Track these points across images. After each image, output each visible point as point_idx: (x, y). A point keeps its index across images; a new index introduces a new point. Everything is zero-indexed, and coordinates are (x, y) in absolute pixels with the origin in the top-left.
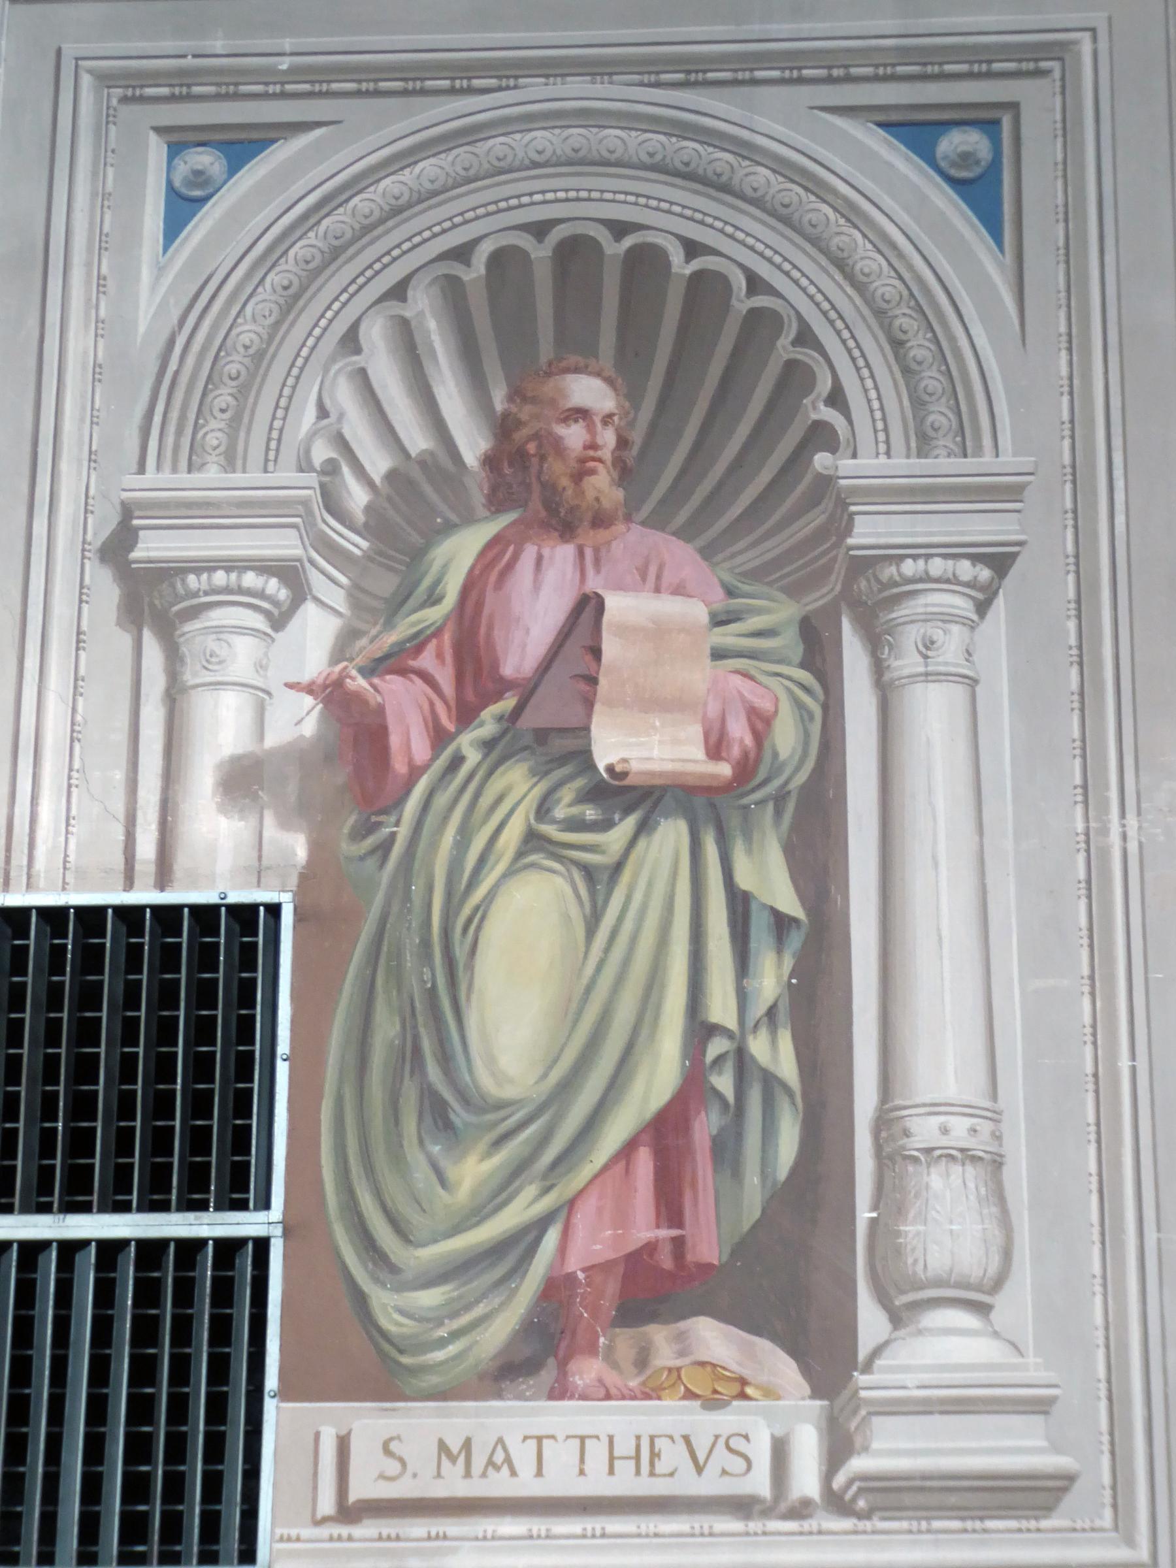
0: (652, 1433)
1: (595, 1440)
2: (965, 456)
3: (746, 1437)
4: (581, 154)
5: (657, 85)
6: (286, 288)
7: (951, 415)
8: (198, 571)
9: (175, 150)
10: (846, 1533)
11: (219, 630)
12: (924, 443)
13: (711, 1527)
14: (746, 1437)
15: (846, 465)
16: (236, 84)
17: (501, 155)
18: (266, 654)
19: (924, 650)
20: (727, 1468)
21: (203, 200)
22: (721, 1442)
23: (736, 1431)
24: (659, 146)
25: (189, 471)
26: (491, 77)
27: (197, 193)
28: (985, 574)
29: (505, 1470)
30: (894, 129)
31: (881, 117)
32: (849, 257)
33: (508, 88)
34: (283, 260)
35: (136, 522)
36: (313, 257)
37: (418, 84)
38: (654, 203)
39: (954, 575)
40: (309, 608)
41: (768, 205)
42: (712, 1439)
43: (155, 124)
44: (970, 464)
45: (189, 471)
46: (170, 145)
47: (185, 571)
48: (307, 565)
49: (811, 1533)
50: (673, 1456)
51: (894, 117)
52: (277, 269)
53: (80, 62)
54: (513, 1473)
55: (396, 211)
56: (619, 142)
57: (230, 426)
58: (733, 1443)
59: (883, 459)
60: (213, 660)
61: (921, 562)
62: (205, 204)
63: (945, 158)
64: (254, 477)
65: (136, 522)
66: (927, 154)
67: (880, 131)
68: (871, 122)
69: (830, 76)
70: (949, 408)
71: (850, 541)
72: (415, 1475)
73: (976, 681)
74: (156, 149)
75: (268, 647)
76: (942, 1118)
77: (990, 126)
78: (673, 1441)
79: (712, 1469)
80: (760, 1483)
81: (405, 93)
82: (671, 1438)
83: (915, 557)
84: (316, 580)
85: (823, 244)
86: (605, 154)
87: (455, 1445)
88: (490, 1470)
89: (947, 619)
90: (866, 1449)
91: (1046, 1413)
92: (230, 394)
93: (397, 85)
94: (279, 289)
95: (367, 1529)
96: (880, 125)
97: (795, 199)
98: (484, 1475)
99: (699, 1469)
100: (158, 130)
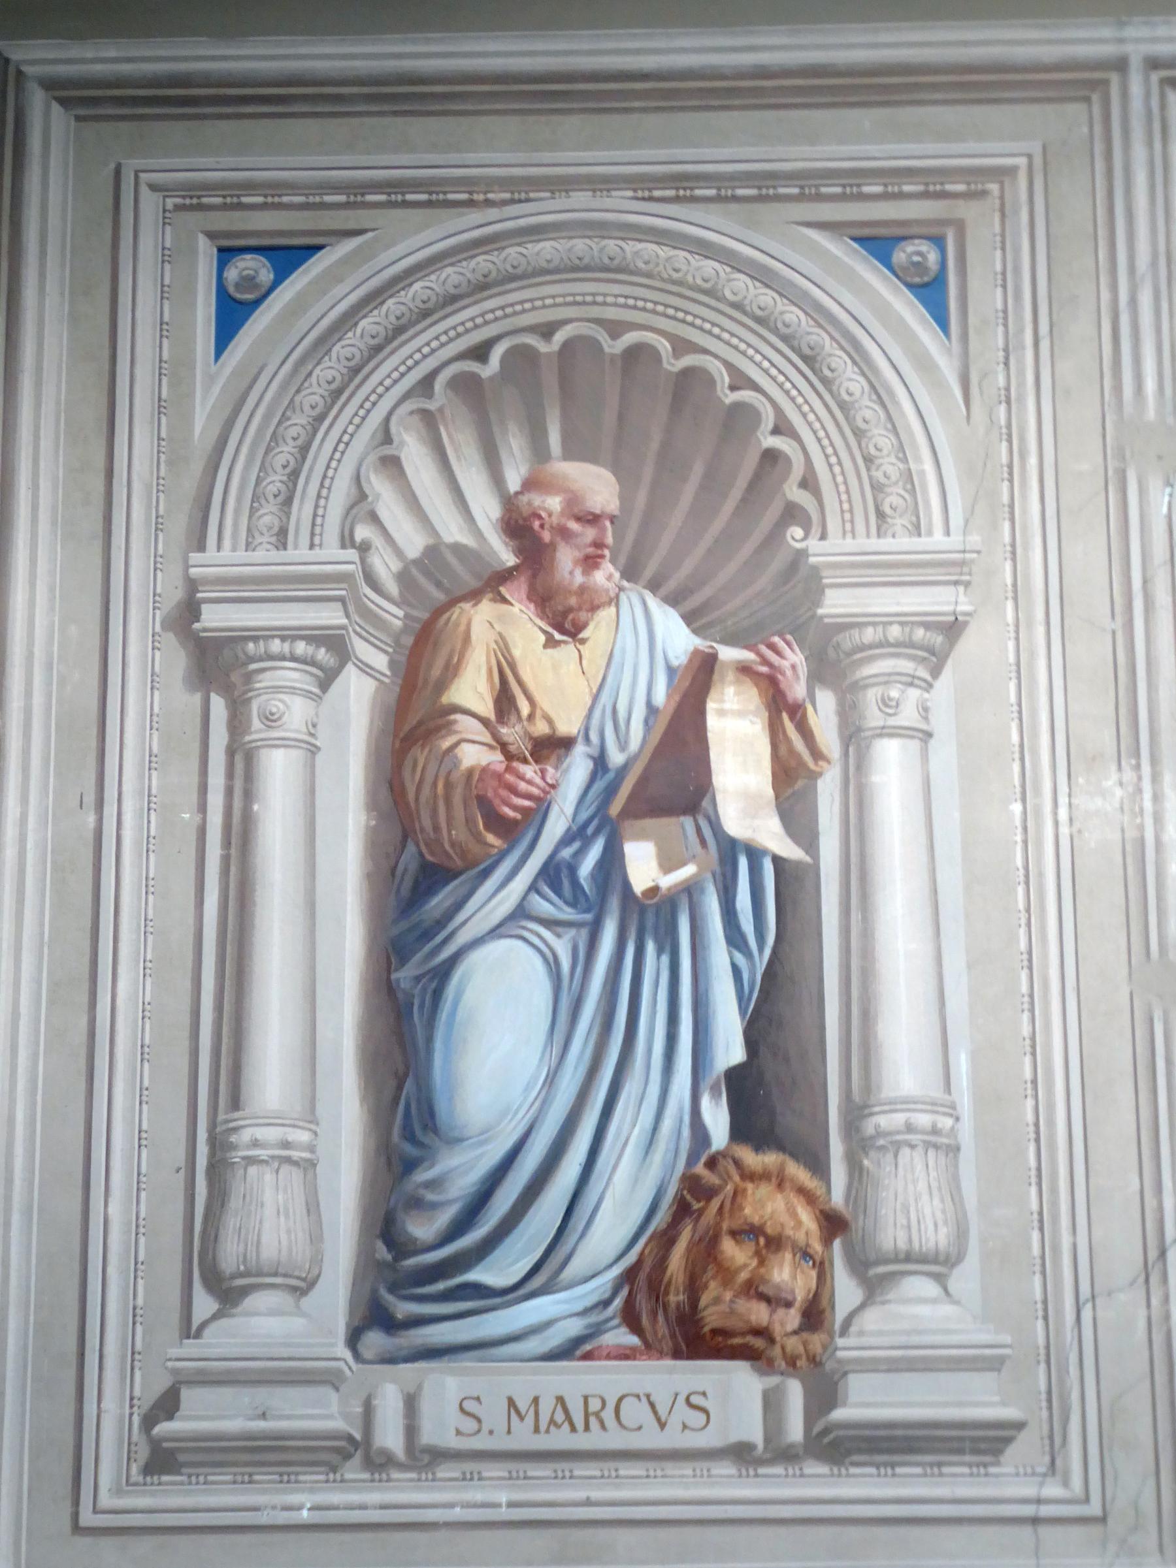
0: (585, 1392)
2: (919, 535)
4: (586, 261)
5: (651, 199)
6: (329, 383)
8: (255, 639)
9: (226, 254)
11: (278, 689)
13: (525, 1472)
15: (813, 544)
18: (317, 715)
21: (258, 302)
22: (681, 1400)
25: (246, 551)
26: (464, 192)
28: (938, 640)
29: (566, 1426)
30: (270, 253)
32: (818, 354)
33: (520, 201)
34: (327, 358)
35: (199, 595)
36: (354, 356)
37: (688, 193)
40: (350, 671)
41: (748, 308)
43: (210, 228)
44: (887, 543)
45: (246, 551)
46: (221, 250)
47: (861, 626)
48: (352, 634)
50: (635, 1412)
51: (866, 232)
53: (142, 175)
54: (573, 1429)
55: (425, 314)
57: (281, 510)
58: (695, 1400)
59: (849, 540)
61: (880, 629)
64: (303, 553)
65: (199, 595)
66: (886, 261)
67: (855, 245)
68: (846, 235)
69: (844, 193)
70: (906, 491)
71: (820, 611)
73: (929, 735)
74: (206, 252)
75: (318, 706)
76: (908, 1115)
77: (938, 241)
78: (640, 1400)
79: (674, 1422)
80: (755, 1434)
81: (429, 204)
82: (638, 1397)
83: (874, 624)
84: (362, 649)
85: (796, 343)
86: (545, 265)
87: (523, 1404)
88: (552, 1428)
89: (292, 691)
90: (844, 1404)
91: (999, 1370)
92: (281, 481)
93: (671, 193)
94: (323, 382)
95: (852, 1479)
98: (547, 1431)
99: (662, 1425)
100: (211, 235)
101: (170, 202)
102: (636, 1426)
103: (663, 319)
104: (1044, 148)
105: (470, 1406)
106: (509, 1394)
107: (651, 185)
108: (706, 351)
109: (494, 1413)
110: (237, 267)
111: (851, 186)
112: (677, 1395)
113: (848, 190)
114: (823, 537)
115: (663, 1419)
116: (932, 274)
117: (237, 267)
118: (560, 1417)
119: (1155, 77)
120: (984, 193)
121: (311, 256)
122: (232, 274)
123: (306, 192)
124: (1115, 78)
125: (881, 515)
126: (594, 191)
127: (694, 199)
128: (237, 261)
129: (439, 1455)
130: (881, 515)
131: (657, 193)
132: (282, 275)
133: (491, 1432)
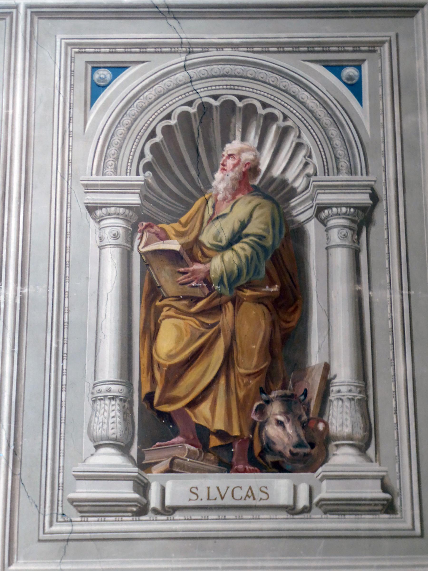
1: (239, 489)
3: (266, 488)
4: (229, 73)
7: (347, 163)
10: (131, 521)
12: (352, 171)
14: (266, 488)
16: (329, 47)
17: (203, 73)
19: (116, 238)
20: (191, 499)
21: (105, 87)
23: (263, 486)
24: (253, 72)
26: (244, 48)
27: (102, 84)
29: (252, 498)
30: (111, 69)
31: (326, 64)
38: (255, 91)
39: (332, 214)
42: (226, 488)
44: (118, 177)
45: (103, 176)
49: (307, 519)
52: (131, 109)
54: (254, 499)
56: (205, 71)
58: (262, 489)
59: (327, 176)
60: (346, 235)
62: (106, 88)
63: (98, 81)
64: (124, 177)
66: (339, 76)
72: (201, 499)
81: (171, 52)
86: (237, 74)
88: (247, 498)
93: (138, 50)
96: (324, 66)
97: (297, 90)
98: (245, 499)
101: (74, 50)
102: (214, 498)
103: (190, 97)
104: (397, 36)
105: (194, 490)
106: (216, 486)
107: (314, 46)
108: (275, 108)
109: (214, 493)
110: (98, 74)
111: (356, 47)
112: (228, 487)
113: (204, 49)
114: (328, 175)
115: (223, 495)
116: (354, 81)
117: (98, 74)
118: (250, 494)
119: (29, 11)
120: (375, 51)
121: (124, 70)
122: (96, 76)
123: (140, 47)
124: (14, 11)
125: (338, 169)
126: (217, 48)
127: (269, 52)
128: (99, 71)
129: (174, 509)
130: (338, 169)
131: (164, 50)
132: (115, 76)
133: (201, 499)
